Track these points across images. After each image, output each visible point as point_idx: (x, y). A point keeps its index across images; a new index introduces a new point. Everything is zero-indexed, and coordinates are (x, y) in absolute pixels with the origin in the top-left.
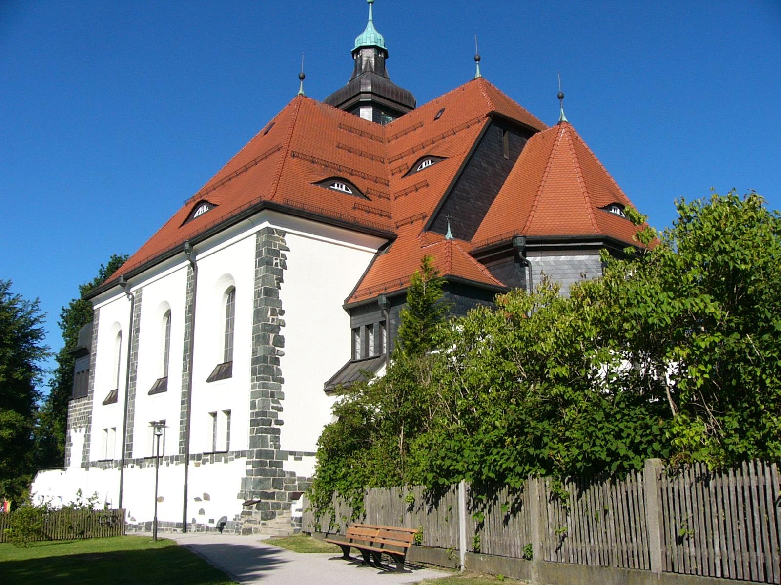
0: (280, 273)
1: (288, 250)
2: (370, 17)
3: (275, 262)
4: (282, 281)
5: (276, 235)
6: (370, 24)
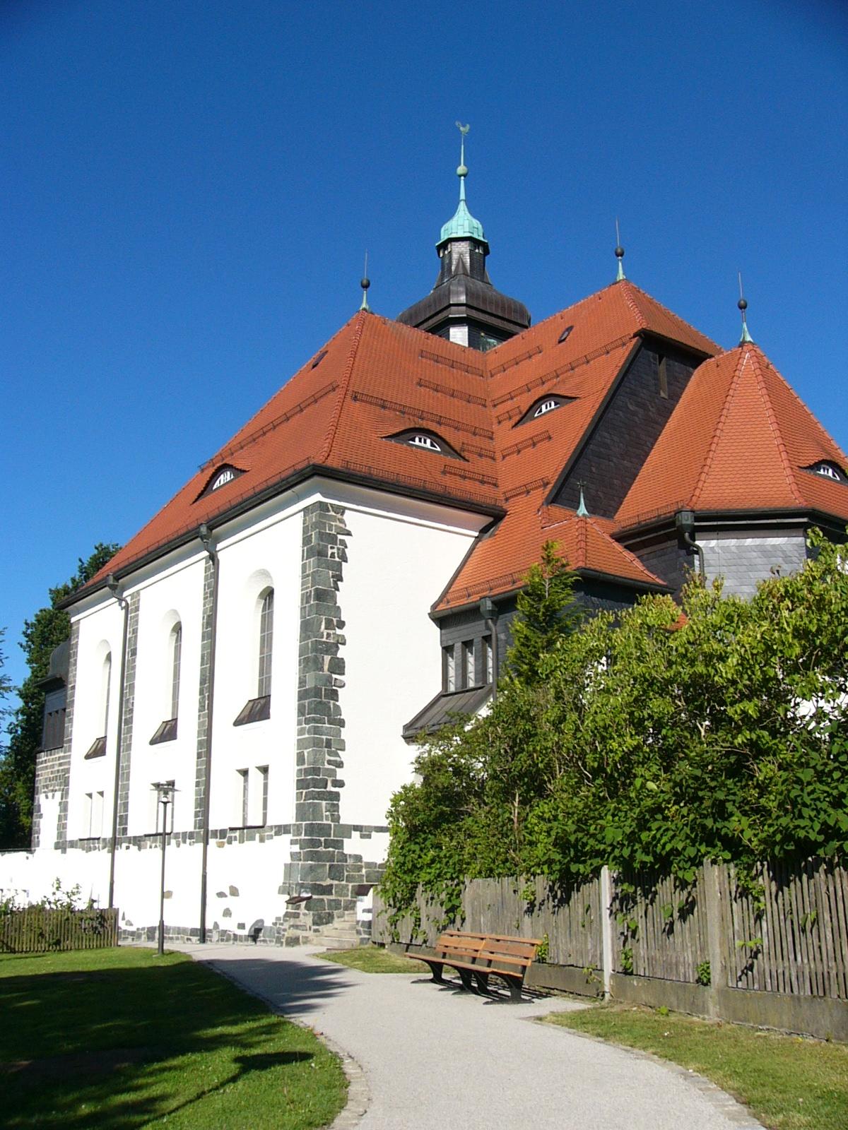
1: (349, 534)
2: (462, 196)
3: (330, 551)
5: (332, 513)
6: (462, 207)
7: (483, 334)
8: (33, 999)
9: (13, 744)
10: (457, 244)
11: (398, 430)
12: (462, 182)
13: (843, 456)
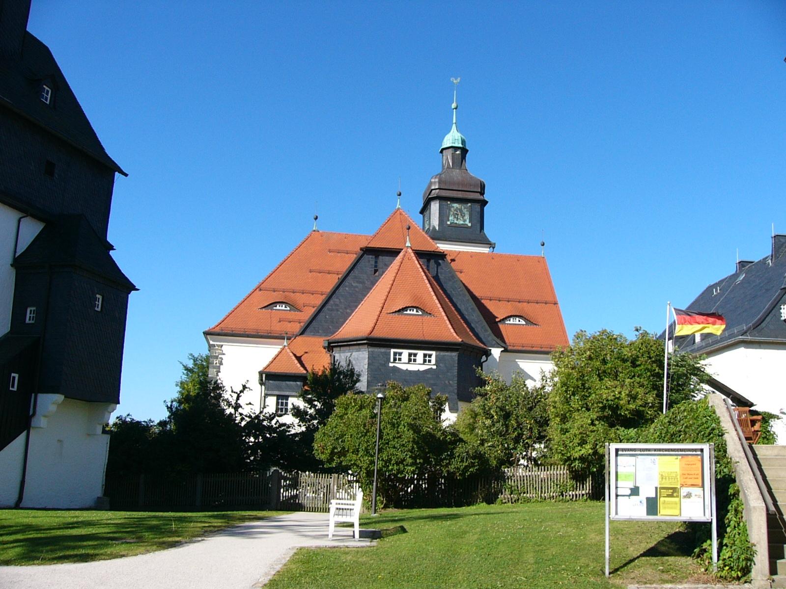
0: (219, 367)
1: (224, 354)
2: (454, 121)
3: (215, 362)
4: (220, 372)
5: (217, 347)
6: (454, 126)
7: (449, 203)
8: (31, 397)
9: (127, 422)
10: (447, 150)
12: (454, 112)
13: (354, 353)
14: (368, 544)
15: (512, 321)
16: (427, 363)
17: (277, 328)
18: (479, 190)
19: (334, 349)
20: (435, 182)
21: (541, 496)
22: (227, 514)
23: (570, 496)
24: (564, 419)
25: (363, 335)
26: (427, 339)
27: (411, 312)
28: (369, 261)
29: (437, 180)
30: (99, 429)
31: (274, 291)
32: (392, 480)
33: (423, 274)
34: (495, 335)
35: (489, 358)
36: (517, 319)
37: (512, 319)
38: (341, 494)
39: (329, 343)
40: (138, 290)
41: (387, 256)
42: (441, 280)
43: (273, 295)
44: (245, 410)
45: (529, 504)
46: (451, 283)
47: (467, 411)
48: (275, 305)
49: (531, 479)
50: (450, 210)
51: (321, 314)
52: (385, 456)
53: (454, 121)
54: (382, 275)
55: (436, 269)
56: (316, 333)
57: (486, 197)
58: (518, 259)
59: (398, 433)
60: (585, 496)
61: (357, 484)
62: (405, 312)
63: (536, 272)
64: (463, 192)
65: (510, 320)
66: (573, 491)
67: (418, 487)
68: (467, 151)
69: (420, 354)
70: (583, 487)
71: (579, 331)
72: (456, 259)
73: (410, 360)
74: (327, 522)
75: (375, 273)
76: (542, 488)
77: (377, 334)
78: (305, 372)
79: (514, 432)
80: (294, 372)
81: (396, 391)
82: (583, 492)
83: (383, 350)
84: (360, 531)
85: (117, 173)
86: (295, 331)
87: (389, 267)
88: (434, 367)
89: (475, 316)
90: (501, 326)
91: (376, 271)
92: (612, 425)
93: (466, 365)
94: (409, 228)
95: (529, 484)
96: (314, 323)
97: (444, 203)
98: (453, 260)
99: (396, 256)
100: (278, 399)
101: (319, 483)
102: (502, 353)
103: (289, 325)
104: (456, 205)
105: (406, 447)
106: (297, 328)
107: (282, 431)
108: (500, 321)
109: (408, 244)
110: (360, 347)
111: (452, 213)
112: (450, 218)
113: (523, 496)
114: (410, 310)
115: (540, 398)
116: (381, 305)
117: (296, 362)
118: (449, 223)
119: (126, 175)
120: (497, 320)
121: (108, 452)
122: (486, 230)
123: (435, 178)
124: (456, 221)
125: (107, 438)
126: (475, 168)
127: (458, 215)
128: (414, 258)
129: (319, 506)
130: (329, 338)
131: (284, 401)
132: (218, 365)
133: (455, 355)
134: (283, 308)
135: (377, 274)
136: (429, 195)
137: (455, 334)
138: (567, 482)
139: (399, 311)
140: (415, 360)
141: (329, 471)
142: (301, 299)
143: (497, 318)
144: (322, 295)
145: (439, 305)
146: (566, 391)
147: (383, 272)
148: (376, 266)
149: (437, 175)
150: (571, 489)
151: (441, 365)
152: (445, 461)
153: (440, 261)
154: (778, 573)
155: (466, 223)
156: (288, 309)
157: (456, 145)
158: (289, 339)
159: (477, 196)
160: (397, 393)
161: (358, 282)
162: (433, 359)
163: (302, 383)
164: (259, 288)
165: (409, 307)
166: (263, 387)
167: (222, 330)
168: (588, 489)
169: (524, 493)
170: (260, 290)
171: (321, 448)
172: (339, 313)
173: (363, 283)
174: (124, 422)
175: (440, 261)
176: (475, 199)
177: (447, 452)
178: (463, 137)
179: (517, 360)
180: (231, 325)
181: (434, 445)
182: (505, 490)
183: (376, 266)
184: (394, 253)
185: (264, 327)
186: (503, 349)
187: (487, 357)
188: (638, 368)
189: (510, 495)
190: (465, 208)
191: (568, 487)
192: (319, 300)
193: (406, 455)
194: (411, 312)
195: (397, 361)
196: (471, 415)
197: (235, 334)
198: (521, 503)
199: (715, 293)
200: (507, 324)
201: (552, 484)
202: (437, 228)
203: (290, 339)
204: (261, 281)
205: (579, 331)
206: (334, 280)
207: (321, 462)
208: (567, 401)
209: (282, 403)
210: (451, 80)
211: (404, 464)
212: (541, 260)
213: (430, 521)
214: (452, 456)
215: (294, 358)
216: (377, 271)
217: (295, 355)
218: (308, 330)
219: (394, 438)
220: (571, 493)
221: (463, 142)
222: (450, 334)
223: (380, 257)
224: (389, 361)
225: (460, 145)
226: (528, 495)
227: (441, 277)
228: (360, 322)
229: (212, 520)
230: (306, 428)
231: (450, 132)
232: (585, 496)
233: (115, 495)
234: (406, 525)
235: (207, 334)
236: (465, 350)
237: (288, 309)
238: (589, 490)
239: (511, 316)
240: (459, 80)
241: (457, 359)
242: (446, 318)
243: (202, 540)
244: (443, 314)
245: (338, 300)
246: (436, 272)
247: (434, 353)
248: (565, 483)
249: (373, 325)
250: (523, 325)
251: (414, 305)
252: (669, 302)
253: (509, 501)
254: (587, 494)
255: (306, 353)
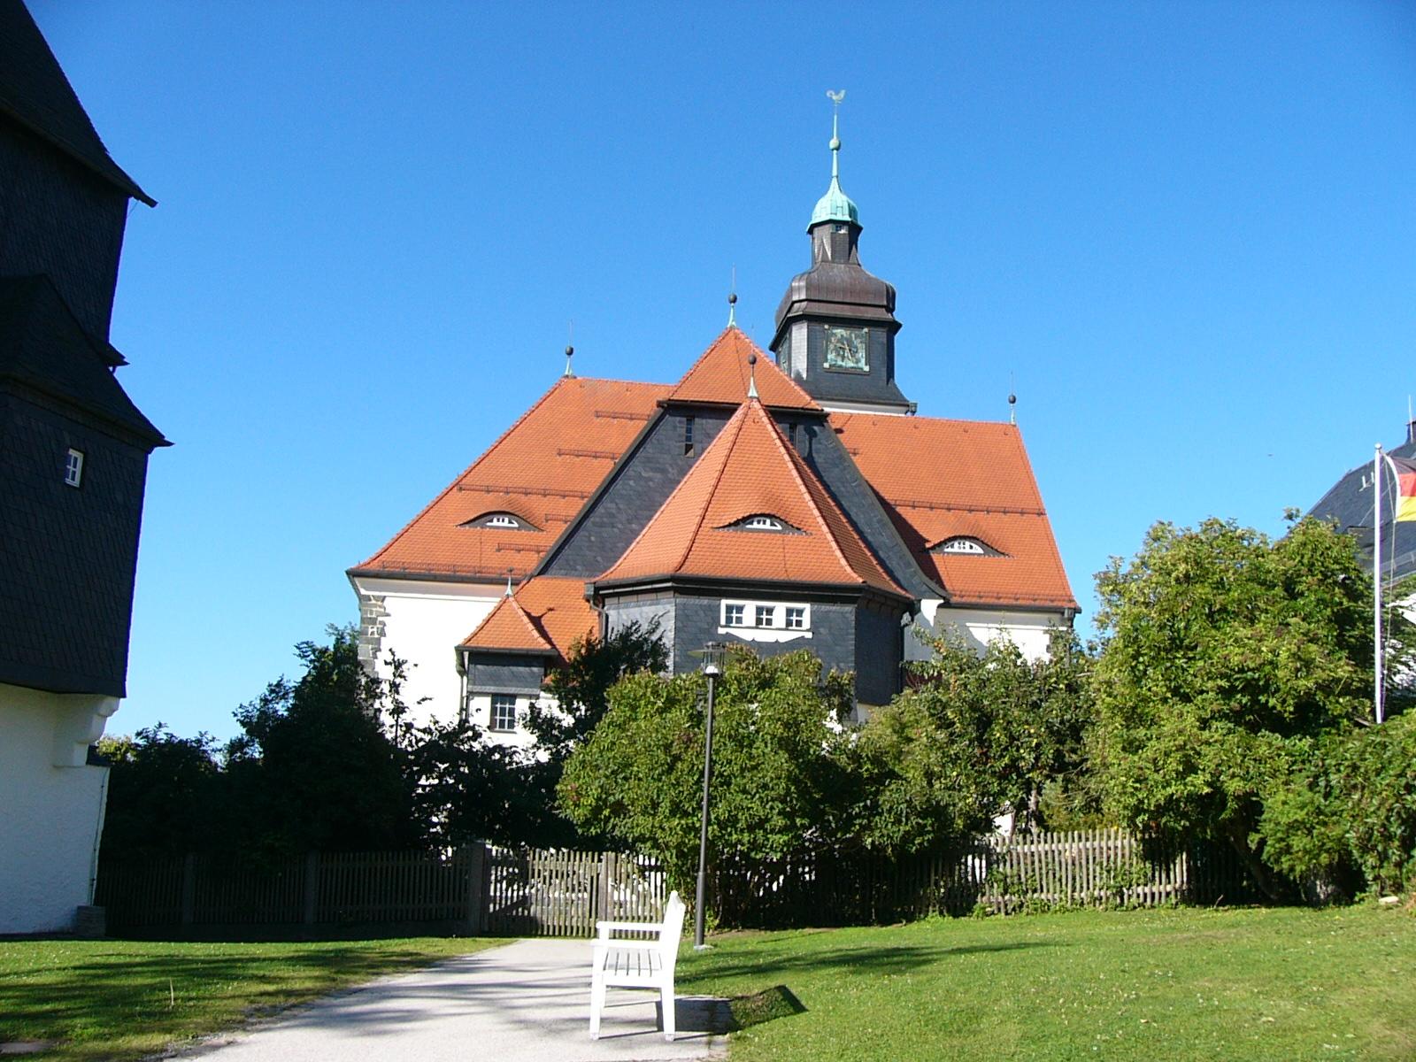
1: (388, 615)
2: (835, 173)
3: (370, 631)
4: (380, 650)
5: (373, 602)
6: (834, 181)
7: (826, 327)
10: (820, 228)
11: (472, 517)
12: (835, 156)
14: (703, 1052)
15: (957, 547)
16: (794, 627)
17: (495, 563)
18: (885, 303)
19: (607, 600)
20: (799, 288)
21: (1073, 898)
22: (351, 951)
23: (1138, 896)
24: (1134, 717)
25: (665, 572)
26: (793, 579)
27: (761, 526)
28: (675, 427)
29: (803, 284)
30: (81, 754)
31: (488, 492)
32: (736, 866)
33: (783, 450)
34: (925, 574)
35: (916, 617)
36: (968, 544)
37: (956, 544)
38: (622, 893)
39: (597, 589)
40: (169, 444)
41: (710, 418)
42: (818, 465)
43: (489, 503)
44: (419, 717)
45: (1047, 916)
46: (836, 470)
47: (884, 720)
48: (490, 517)
49: (1050, 860)
50: (828, 340)
51: (581, 533)
52: (722, 809)
53: (835, 173)
54: (701, 454)
55: (807, 443)
56: (570, 571)
57: (898, 316)
58: (966, 429)
59: (751, 758)
60: (1172, 896)
61: (659, 874)
62: (748, 526)
63: (1003, 453)
64: (853, 307)
65: (952, 546)
66: (1146, 885)
67: (794, 879)
68: (860, 229)
69: (780, 608)
70: (1168, 876)
71: (1156, 524)
72: (844, 429)
73: (759, 621)
74: (586, 971)
75: (687, 452)
76: (1074, 879)
77: (694, 569)
78: (548, 647)
79: (1002, 756)
80: (525, 647)
81: (744, 665)
82: (1169, 888)
83: (705, 601)
84: (677, 1002)
85: (132, 200)
86: (528, 568)
87: (714, 438)
88: (809, 635)
89: (887, 537)
90: (935, 556)
91: (689, 447)
92: (1254, 728)
93: (874, 629)
94: (754, 362)
95: (1044, 871)
96: (567, 551)
97: (817, 327)
98: (839, 431)
99: (729, 419)
100: (494, 702)
101: (574, 873)
102: (940, 610)
103: (518, 556)
104: (840, 332)
105: (773, 789)
106: (533, 561)
107: (492, 766)
108: (933, 548)
109: (753, 393)
110: (660, 595)
111: (832, 347)
112: (829, 357)
113: (1032, 899)
114: (759, 522)
115: (1055, 682)
116: (700, 512)
117: (531, 626)
118: (826, 365)
119: (152, 203)
120: (928, 545)
121: (104, 806)
122: (898, 379)
123: (800, 280)
124: (840, 363)
125: (102, 775)
126: (876, 261)
127: (844, 349)
128: (765, 420)
129: (574, 924)
130: (597, 579)
131: (507, 706)
132: (376, 636)
133: (849, 610)
134: (506, 524)
135: (691, 453)
136: (789, 311)
137: (848, 569)
138: (1131, 865)
139: (736, 523)
140: (769, 622)
141: (596, 845)
142: (539, 507)
143: (928, 541)
144: (583, 498)
145: (816, 512)
146: (1135, 657)
147: (703, 450)
148: (689, 439)
149: (803, 275)
150: (1142, 881)
151: (822, 630)
152: (858, 821)
153: (816, 428)
154: (89, 766)
155: (860, 365)
156: (516, 525)
157: (839, 217)
158: (515, 583)
159: (882, 314)
160: (747, 669)
161: (652, 469)
162: (806, 620)
163: (543, 670)
164: (459, 486)
165: (756, 515)
166: (465, 678)
167: (384, 567)
168: (1178, 880)
169: (1035, 891)
170: (461, 489)
171: (575, 799)
172: (615, 530)
173: (663, 471)
174: (153, 742)
175: (816, 428)
176: (878, 320)
177: (865, 801)
178: (851, 202)
179: (968, 624)
180: (406, 557)
181: (831, 787)
182: (992, 886)
183: (689, 439)
184: (723, 411)
185: (467, 561)
186: (942, 601)
187: (912, 616)
188: (1301, 601)
189: (1003, 895)
190: (858, 337)
191: (1135, 876)
192: (574, 508)
193: (772, 808)
194: (761, 526)
195: (734, 624)
196: (892, 726)
197: (410, 574)
198: (1028, 914)
199: (1365, 486)
200: (948, 553)
201: (1098, 868)
202: (805, 376)
203: (517, 584)
204: (462, 473)
205: (1156, 524)
206: (606, 468)
207: (567, 824)
208: (1137, 681)
209: (503, 710)
210: (828, 94)
211: (765, 830)
212: (1009, 431)
213: (853, 973)
214: (874, 810)
215: (526, 619)
216: (691, 448)
217: (528, 615)
218: (555, 565)
219: (742, 770)
220: (1140, 890)
221: (852, 212)
222: (838, 569)
223: (696, 420)
224: (717, 623)
225: (847, 218)
226: (1043, 896)
227: (819, 459)
228: (657, 546)
229: (285, 971)
230: (551, 754)
231: (826, 193)
232: (1172, 896)
233: (120, 904)
234: (796, 983)
235: (353, 574)
236: (870, 600)
237: (516, 525)
238: (1182, 882)
239: (954, 538)
240: (842, 94)
241: (853, 618)
242: (830, 537)
243: (229, 1044)
244: (825, 528)
245: (614, 506)
246: (807, 450)
247: (807, 607)
248: (1127, 867)
249: (684, 552)
250: (979, 555)
251: (767, 512)
252: (1378, 446)
253: (999, 910)
254: (1176, 891)
255: (551, 610)
